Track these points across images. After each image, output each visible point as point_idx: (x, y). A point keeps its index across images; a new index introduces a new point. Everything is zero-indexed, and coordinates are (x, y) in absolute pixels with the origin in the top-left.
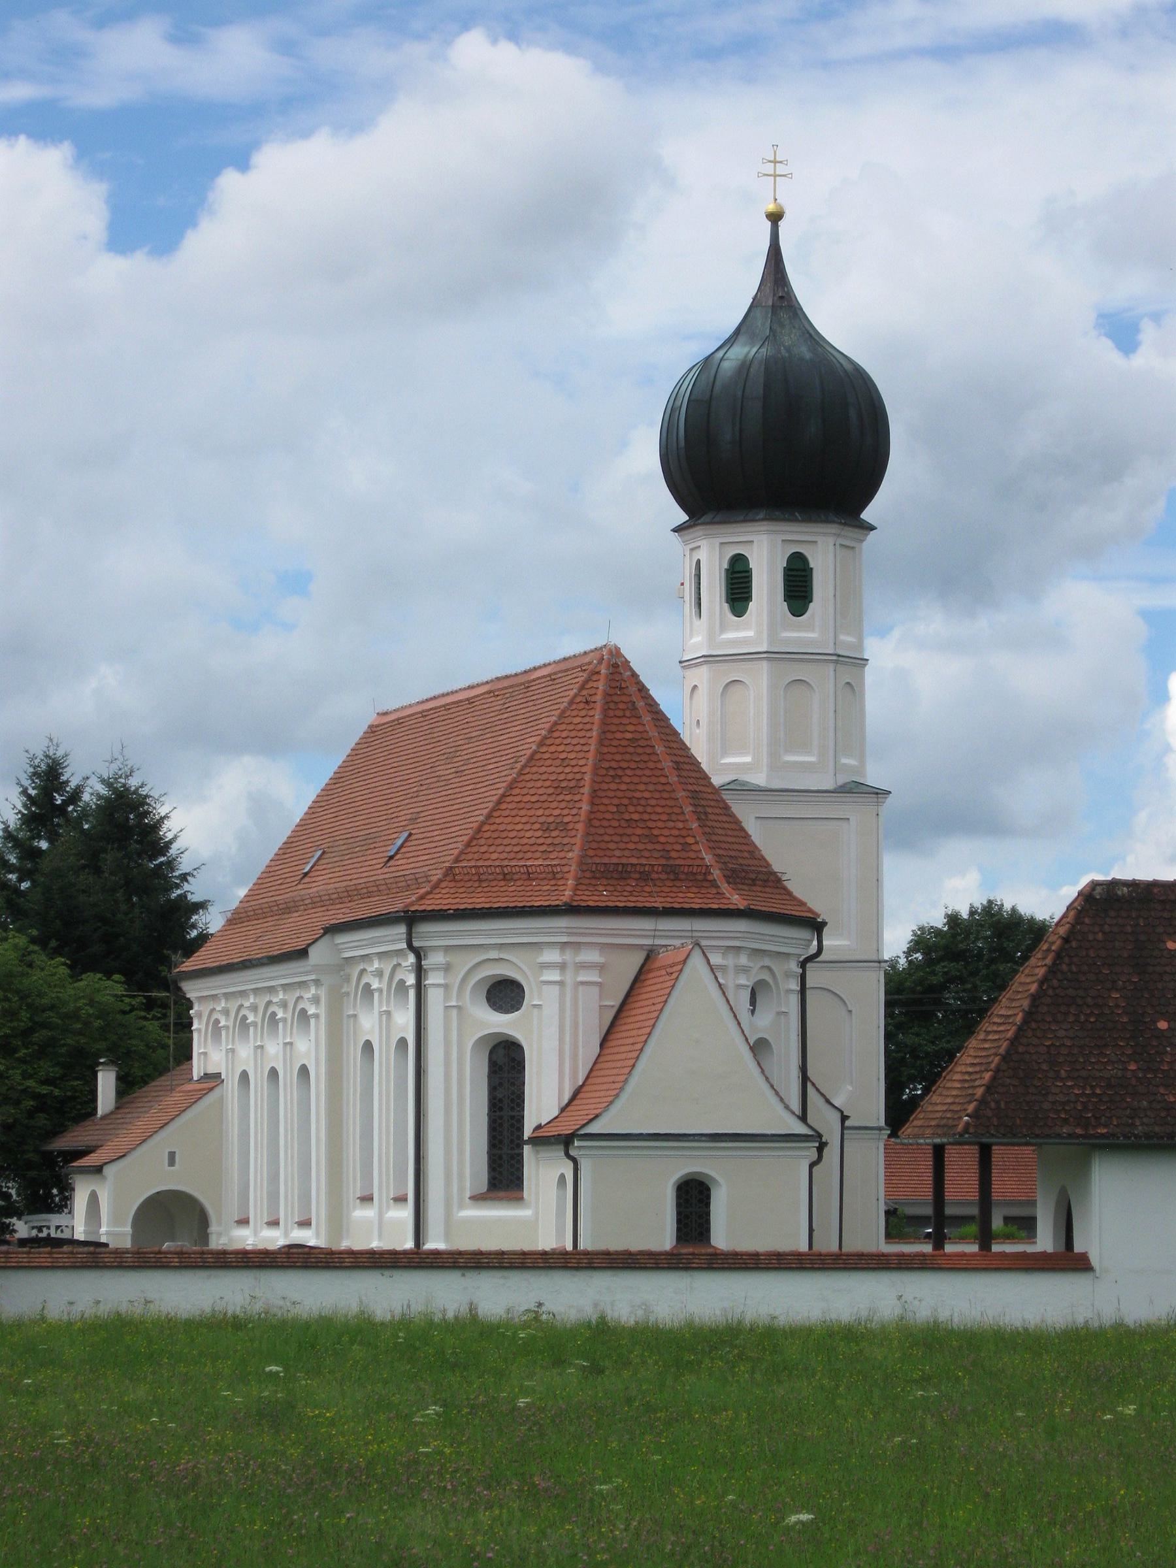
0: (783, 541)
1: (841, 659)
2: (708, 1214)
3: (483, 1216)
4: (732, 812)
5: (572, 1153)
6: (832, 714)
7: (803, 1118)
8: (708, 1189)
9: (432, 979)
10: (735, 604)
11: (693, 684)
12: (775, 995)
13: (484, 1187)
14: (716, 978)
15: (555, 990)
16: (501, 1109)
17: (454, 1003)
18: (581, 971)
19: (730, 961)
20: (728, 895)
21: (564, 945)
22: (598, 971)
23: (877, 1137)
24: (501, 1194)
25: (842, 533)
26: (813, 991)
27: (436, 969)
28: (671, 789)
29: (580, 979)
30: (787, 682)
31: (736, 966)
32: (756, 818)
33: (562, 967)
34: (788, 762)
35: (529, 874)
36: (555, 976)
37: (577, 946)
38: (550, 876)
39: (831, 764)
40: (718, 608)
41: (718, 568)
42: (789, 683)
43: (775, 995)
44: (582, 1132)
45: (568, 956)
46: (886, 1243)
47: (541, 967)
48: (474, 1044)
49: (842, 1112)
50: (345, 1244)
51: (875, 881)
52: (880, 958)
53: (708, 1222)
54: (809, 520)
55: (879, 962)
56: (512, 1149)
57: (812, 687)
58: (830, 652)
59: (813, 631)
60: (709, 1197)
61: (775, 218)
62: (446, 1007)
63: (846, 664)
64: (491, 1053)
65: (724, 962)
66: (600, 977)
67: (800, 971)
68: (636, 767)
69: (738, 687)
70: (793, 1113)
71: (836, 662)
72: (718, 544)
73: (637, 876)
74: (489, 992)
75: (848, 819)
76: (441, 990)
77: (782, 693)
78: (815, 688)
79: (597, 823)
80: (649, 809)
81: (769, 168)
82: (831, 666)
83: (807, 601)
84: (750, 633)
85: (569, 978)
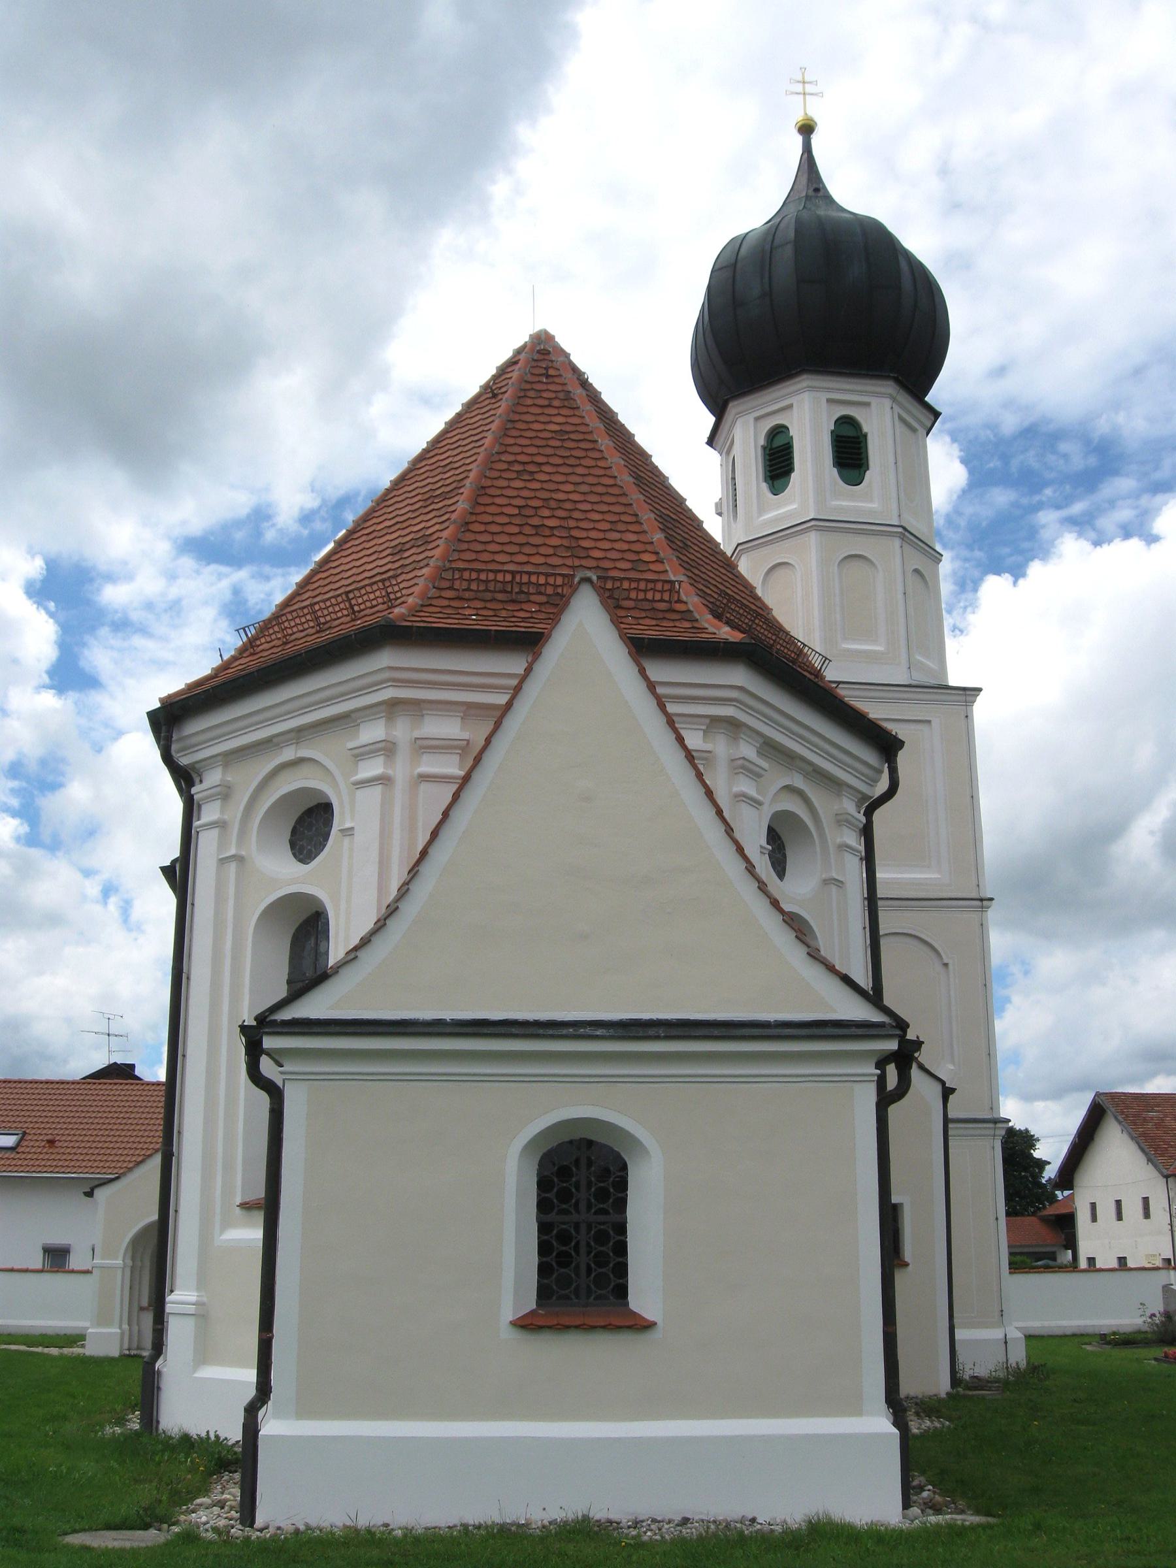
0: (829, 401)
2: (622, 1229)
4: (738, 571)
5: (267, 1067)
6: (900, 596)
7: (875, 997)
8: (624, 1167)
9: (209, 814)
10: (775, 483)
12: (818, 849)
14: (680, 740)
19: (721, 747)
20: (711, 630)
21: (393, 707)
22: (457, 757)
23: (992, 1132)
26: (892, 939)
27: (210, 799)
28: (621, 493)
29: (424, 769)
30: (840, 558)
31: (732, 760)
33: (387, 749)
34: (848, 650)
37: (416, 708)
39: (904, 656)
40: (754, 488)
41: (752, 444)
42: (843, 560)
43: (818, 849)
44: (286, 1015)
45: (402, 731)
46: (1010, 1273)
49: (943, 1083)
51: (969, 798)
52: (983, 895)
53: (622, 1249)
55: (981, 900)
58: (896, 524)
59: (871, 501)
60: (622, 1185)
61: (807, 130)
65: (708, 746)
67: (864, 820)
68: (562, 462)
69: (781, 572)
70: (847, 980)
71: (902, 537)
72: (752, 421)
73: (543, 599)
74: (300, 821)
75: (929, 722)
77: (836, 568)
78: (879, 566)
79: (476, 527)
80: (577, 515)
81: (799, 88)
83: (863, 469)
84: (795, 506)
85: (401, 771)
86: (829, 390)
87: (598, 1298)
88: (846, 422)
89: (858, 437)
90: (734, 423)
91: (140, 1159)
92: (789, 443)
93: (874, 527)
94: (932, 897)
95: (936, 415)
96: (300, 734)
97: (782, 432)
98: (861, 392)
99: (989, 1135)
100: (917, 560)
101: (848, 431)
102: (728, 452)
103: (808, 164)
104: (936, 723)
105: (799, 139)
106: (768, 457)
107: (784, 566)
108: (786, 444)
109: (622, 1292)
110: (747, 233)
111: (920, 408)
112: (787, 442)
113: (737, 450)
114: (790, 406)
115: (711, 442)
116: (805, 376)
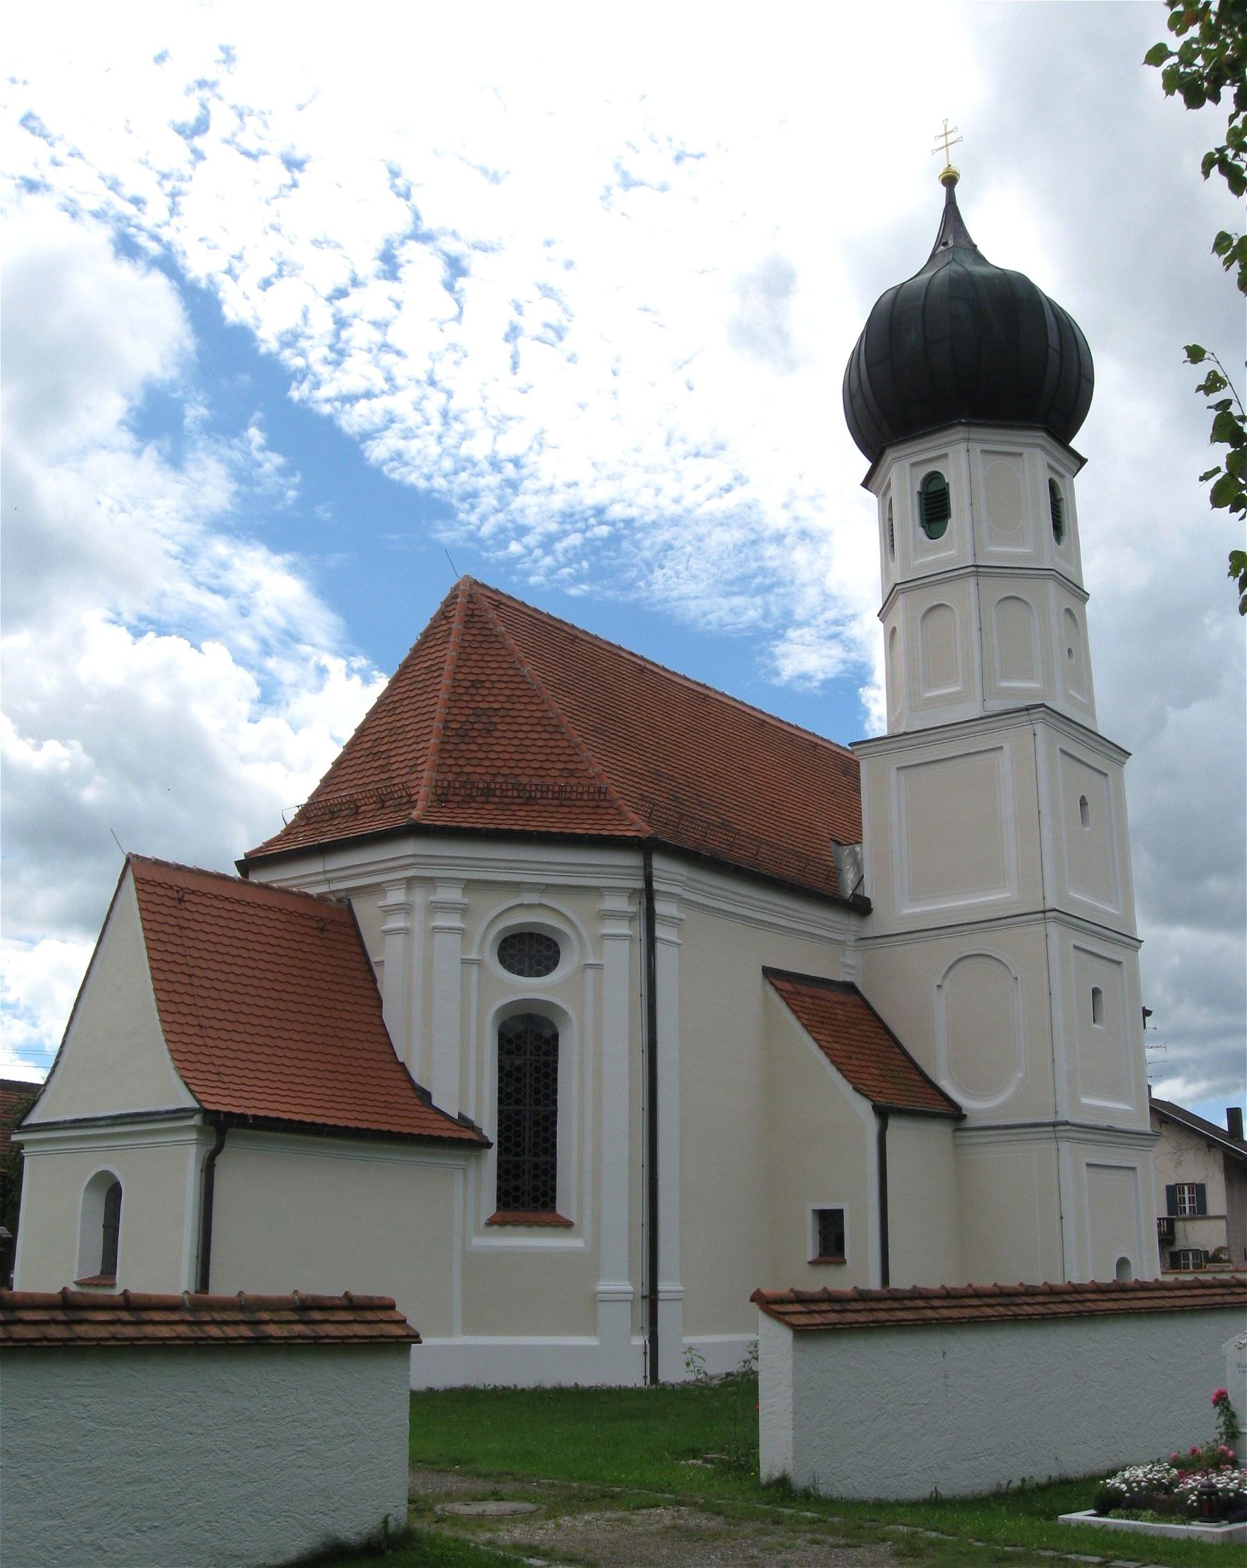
0: (983, 451)
1: (980, 570)
17: (474, 956)
25: (972, 436)
32: (898, 769)
34: (928, 698)
36: (454, 921)
47: (436, 908)
50: (659, 1303)
54: (1012, 427)
57: (953, 610)
61: (950, 181)
62: (465, 962)
66: (462, 923)
71: (976, 574)
76: (456, 938)
82: (972, 581)
87: (515, 1207)
90: (890, 467)
92: (944, 489)
93: (1029, 572)
94: (973, 921)
95: (1082, 461)
96: (548, 888)
97: (936, 478)
99: (1051, 1138)
100: (1070, 602)
102: (884, 495)
106: (924, 502)
107: (1016, 601)
108: (941, 490)
109: (554, 1208)
110: (903, 284)
111: (1065, 453)
112: (942, 487)
113: (893, 493)
114: (946, 455)
115: (865, 484)
116: (1042, 434)
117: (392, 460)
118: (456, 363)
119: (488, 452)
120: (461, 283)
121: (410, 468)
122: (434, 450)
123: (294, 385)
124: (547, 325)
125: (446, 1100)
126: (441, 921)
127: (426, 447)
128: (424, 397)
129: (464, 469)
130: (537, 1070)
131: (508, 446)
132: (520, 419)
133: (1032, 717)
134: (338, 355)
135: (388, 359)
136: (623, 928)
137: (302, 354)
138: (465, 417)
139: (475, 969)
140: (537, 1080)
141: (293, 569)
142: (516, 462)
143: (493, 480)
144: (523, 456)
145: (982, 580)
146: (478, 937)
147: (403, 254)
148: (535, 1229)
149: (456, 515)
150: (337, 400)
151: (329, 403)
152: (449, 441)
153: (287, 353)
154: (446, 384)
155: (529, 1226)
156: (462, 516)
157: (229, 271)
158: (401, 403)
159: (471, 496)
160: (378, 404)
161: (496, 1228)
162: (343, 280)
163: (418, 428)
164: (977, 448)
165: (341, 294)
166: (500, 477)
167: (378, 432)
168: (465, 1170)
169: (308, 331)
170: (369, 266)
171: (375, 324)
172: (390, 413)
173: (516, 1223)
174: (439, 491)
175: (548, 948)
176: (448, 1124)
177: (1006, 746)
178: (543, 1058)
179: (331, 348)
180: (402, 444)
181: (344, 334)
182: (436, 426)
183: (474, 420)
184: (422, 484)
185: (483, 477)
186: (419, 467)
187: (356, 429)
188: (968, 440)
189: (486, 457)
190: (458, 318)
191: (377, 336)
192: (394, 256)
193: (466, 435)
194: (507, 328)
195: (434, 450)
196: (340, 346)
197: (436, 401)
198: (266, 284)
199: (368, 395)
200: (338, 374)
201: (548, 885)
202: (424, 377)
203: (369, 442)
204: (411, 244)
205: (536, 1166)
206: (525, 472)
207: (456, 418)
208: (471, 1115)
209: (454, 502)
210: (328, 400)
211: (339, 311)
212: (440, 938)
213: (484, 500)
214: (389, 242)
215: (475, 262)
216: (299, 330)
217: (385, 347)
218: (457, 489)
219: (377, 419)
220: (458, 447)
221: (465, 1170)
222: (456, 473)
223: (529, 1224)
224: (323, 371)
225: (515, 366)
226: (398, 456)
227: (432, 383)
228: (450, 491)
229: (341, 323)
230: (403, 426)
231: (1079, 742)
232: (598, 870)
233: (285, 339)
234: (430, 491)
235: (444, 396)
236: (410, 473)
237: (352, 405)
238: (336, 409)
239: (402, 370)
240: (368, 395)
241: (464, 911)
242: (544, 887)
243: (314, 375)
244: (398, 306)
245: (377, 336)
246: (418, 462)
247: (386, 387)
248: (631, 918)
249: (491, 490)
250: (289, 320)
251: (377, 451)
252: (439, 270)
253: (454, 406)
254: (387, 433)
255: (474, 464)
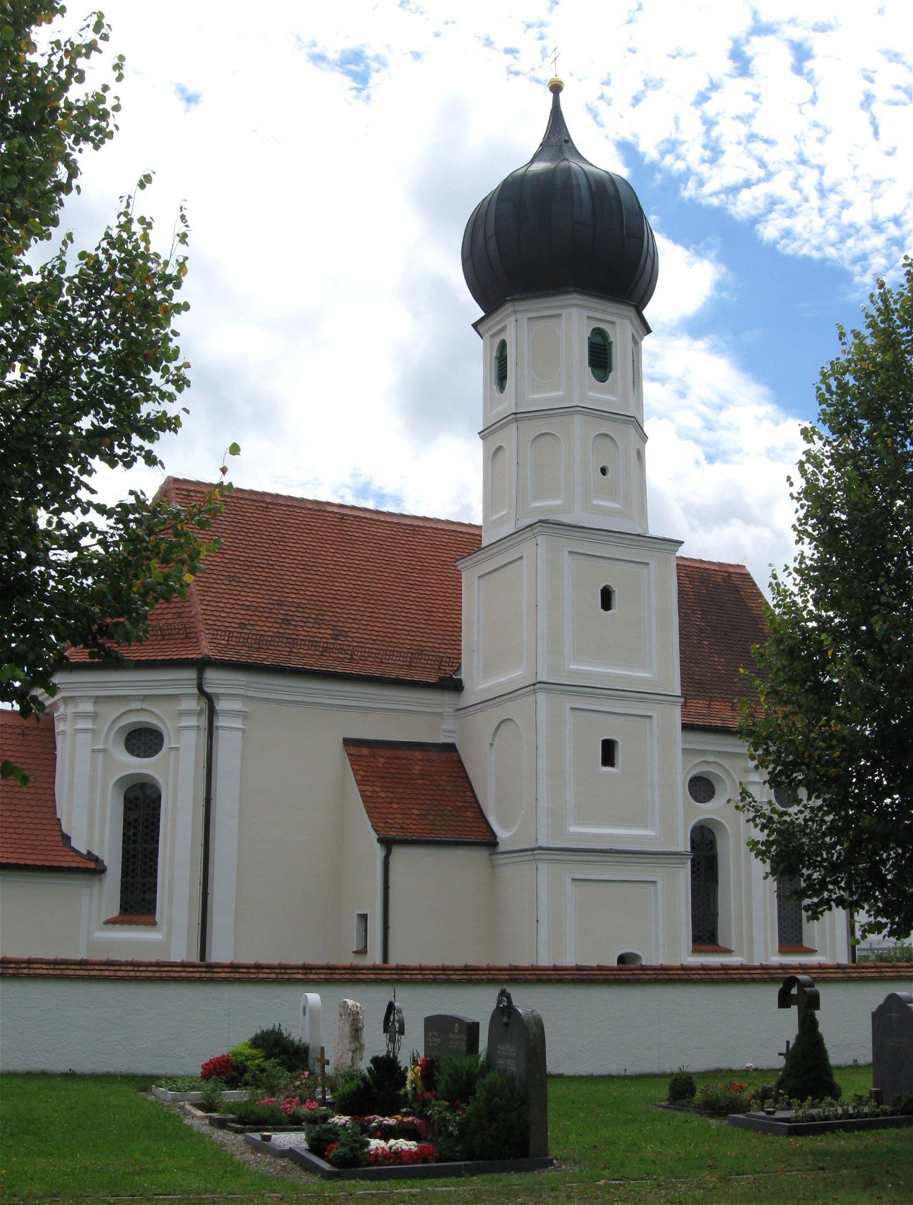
0: (529, 319)
1: (518, 416)
3: (130, 939)
11: (500, 444)
13: (115, 911)
15: (87, 737)
16: (135, 842)
17: (100, 746)
18: (183, 717)
24: (135, 918)
35: (187, 633)
36: (88, 725)
38: (160, 638)
48: (119, 779)
50: (539, 964)
54: (536, 297)
56: (145, 877)
61: (556, 88)
62: (93, 751)
63: (528, 419)
64: (126, 791)
71: (516, 420)
74: (129, 734)
75: (647, 564)
76: (89, 736)
86: (589, 309)
88: (599, 333)
89: (605, 346)
91: (472, 552)
96: (145, 698)
98: (551, 308)
101: (599, 340)
103: (556, 116)
104: (652, 566)
105: (551, 95)
114: (560, 315)
116: (575, 295)
117: (782, 238)
118: (820, 140)
119: (870, 217)
120: (808, 65)
121: (799, 243)
122: (818, 223)
123: (682, 186)
124: (897, 88)
125: (80, 844)
126: (81, 725)
127: (811, 221)
128: (798, 176)
129: (849, 236)
130: (147, 820)
131: (885, 209)
132: (892, 181)
133: (534, 531)
134: (714, 153)
135: (759, 148)
136: (193, 722)
137: (679, 157)
138: (840, 188)
139: (101, 755)
140: (147, 827)
141: (714, 350)
142: (897, 221)
143: (877, 241)
144: (901, 215)
145: (521, 424)
146: (104, 733)
147: (748, 50)
148: (134, 927)
149: (852, 279)
150: (721, 192)
151: (714, 196)
152: (831, 212)
153: (669, 159)
154: (814, 161)
155: (130, 924)
156: (857, 279)
157: (602, 97)
158: (780, 186)
159: (863, 258)
160: (759, 191)
161: (110, 926)
162: (703, 85)
163: (798, 207)
164: (523, 317)
165: (703, 98)
166: (883, 237)
167: (762, 216)
168: (91, 888)
169: (681, 138)
170: (725, 66)
171: (739, 118)
172: (771, 197)
173: (130, 923)
174: (832, 260)
175: (156, 738)
176: (78, 859)
177: (525, 555)
178: (151, 812)
179: (705, 147)
180: (787, 223)
181: (714, 134)
182: (815, 201)
183: (850, 190)
184: (816, 255)
185: (868, 240)
186: (808, 240)
187: (744, 215)
188: (515, 312)
189: (867, 221)
190: (814, 100)
191: (743, 130)
192: (743, 53)
193: (845, 205)
194: (862, 98)
195: (818, 223)
196: (711, 144)
197: (810, 178)
198: (636, 100)
199: (747, 184)
200: (715, 170)
201: (145, 696)
202: (794, 158)
203: (758, 226)
204: (754, 39)
205: (144, 885)
206: (906, 228)
207: (832, 190)
208: (96, 852)
209: (847, 265)
210: (715, 194)
211: (704, 112)
212: (79, 736)
213: (874, 261)
214: (736, 42)
215: (818, 43)
216: (673, 137)
217: (752, 137)
218: (847, 256)
219: (760, 204)
220: (839, 217)
221: (91, 888)
222: (842, 241)
223: (138, 923)
224: (704, 169)
225: (876, 133)
226: (787, 234)
227: (803, 161)
228: (841, 258)
229: (709, 123)
230: (783, 207)
231: (500, 553)
232: (173, 683)
233: (662, 148)
234: (823, 261)
235: (816, 172)
236: (801, 247)
237: (734, 196)
238: (722, 200)
239: (770, 155)
240: (747, 184)
241: (94, 717)
242: (142, 697)
243: (697, 174)
244: (756, 98)
245: (743, 130)
246: (806, 235)
247: (761, 173)
248: (199, 714)
249: (878, 251)
250: (666, 131)
251: (769, 231)
252: (787, 58)
253: (827, 182)
254: (773, 216)
255: (858, 230)
